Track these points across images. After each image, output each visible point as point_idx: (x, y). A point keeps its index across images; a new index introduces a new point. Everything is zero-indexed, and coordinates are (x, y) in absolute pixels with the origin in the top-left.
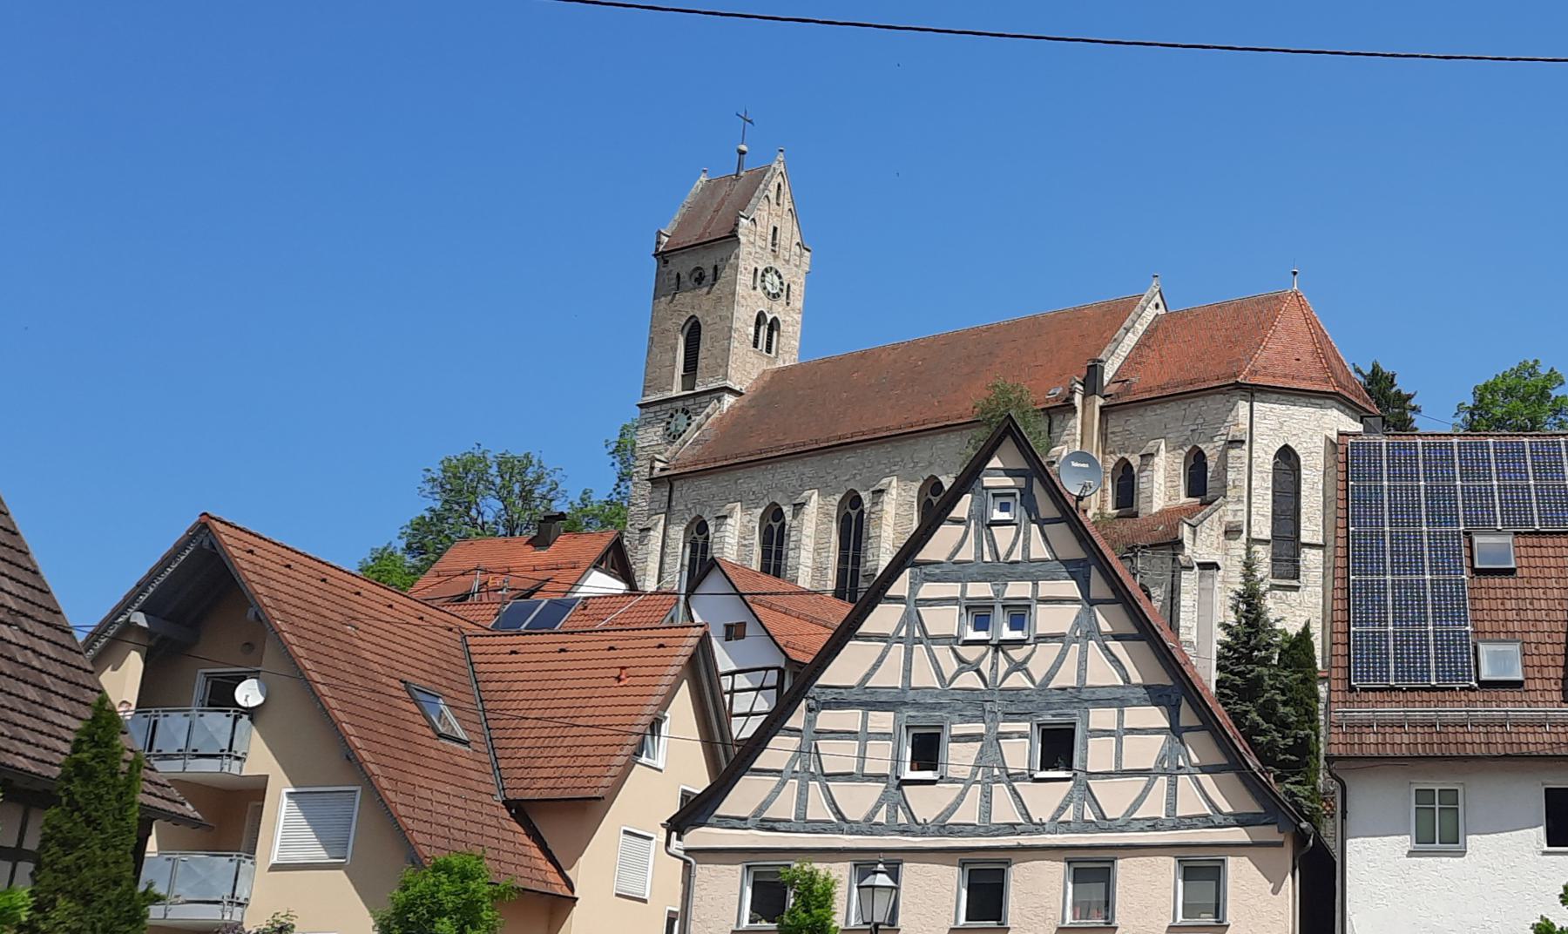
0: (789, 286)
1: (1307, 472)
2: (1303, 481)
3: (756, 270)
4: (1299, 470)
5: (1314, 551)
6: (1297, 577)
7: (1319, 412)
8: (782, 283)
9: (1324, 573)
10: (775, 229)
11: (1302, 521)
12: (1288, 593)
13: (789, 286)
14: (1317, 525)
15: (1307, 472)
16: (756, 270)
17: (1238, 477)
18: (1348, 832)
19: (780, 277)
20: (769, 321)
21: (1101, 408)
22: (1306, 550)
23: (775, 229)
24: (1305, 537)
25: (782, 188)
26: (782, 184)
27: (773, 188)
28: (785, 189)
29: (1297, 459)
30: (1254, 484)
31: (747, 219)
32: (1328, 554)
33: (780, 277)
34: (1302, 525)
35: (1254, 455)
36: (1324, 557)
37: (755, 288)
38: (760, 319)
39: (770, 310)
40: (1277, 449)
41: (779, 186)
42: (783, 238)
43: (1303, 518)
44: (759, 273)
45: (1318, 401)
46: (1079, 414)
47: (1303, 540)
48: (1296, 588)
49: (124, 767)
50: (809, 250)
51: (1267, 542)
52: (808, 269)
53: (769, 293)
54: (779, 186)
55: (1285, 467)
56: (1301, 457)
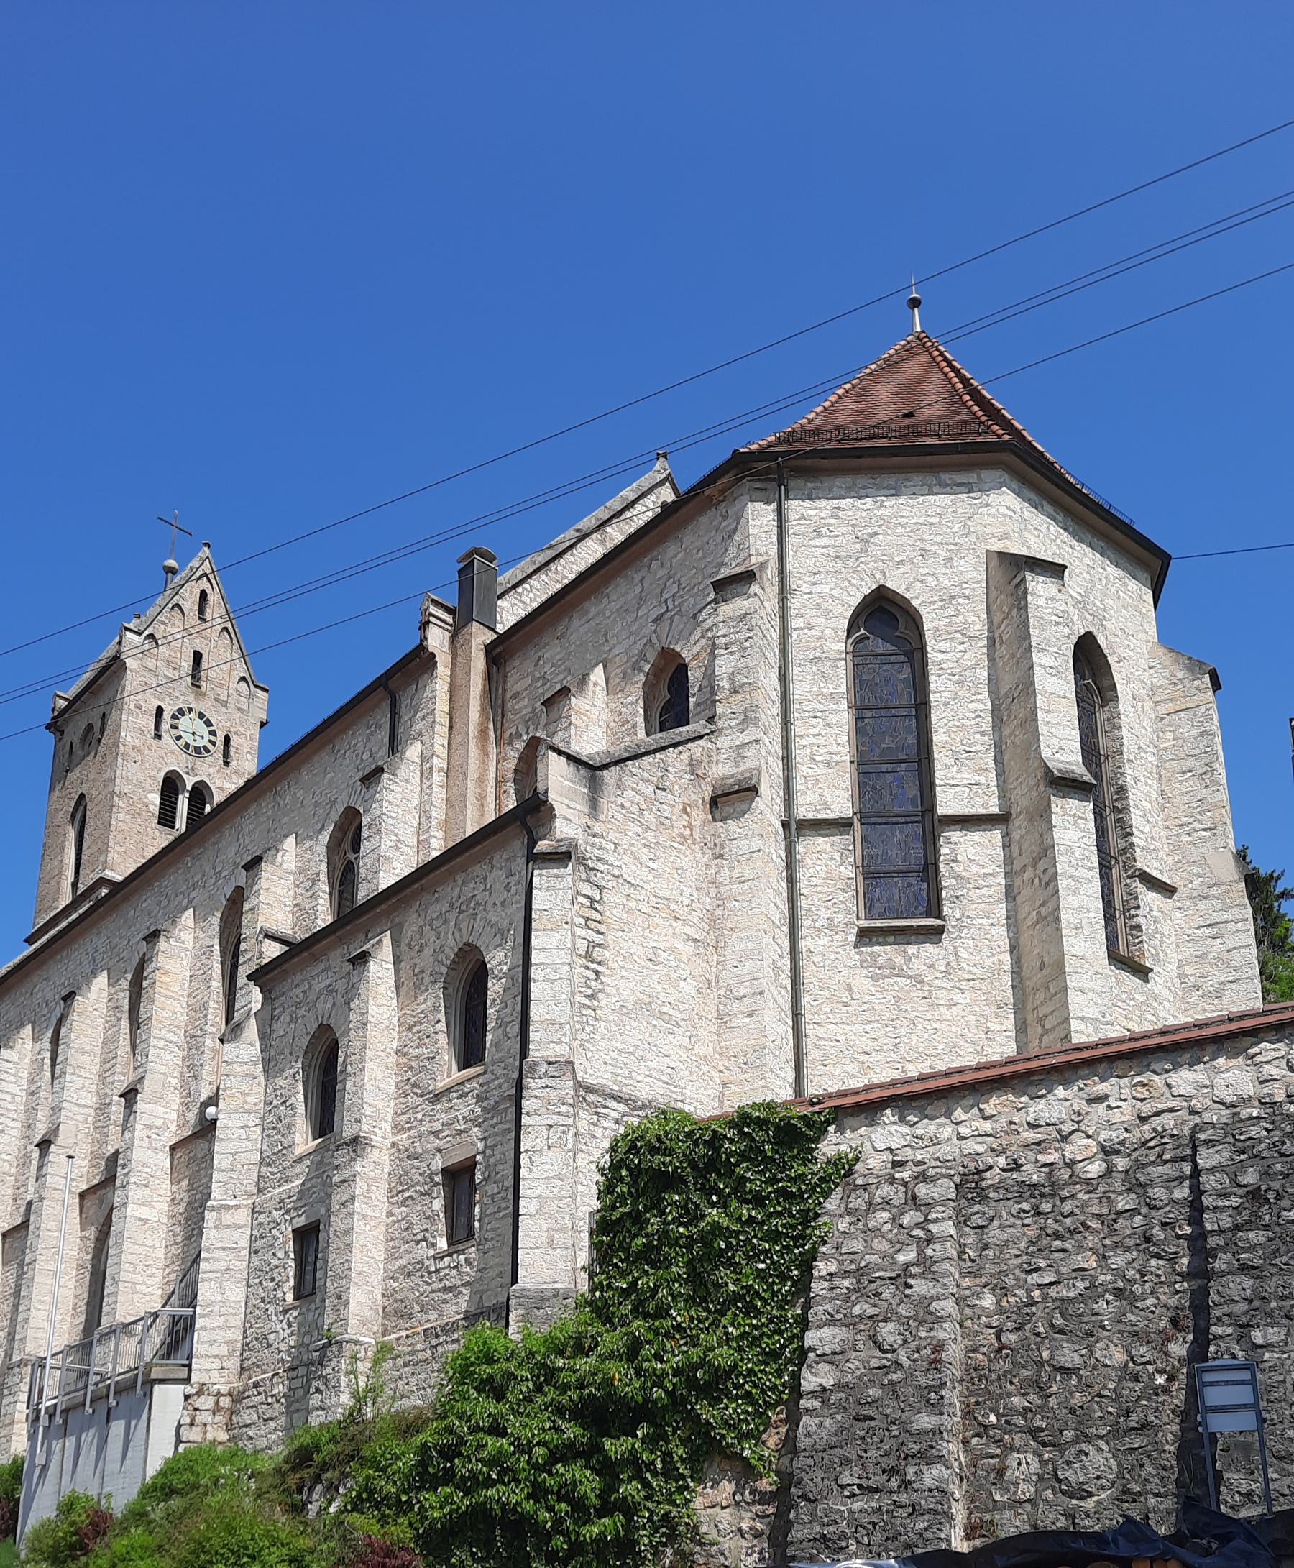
0: (227, 739)
1: (941, 646)
2: (932, 669)
3: (160, 711)
4: (922, 648)
5: (977, 836)
6: (934, 908)
7: (964, 501)
8: (213, 733)
9: (1009, 888)
10: (198, 657)
11: (938, 765)
12: (912, 949)
13: (227, 739)
14: (979, 771)
15: (941, 646)
16: (160, 711)
17: (743, 662)
18: (111, 1417)
19: (208, 723)
20: (189, 787)
21: (489, 649)
22: (955, 835)
23: (198, 657)
24: (948, 803)
25: (210, 597)
26: (209, 591)
27: (189, 599)
28: (214, 598)
29: (914, 620)
30: (796, 690)
31: (140, 634)
32: (1016, 835)
33: (208, 723)
34: (939, 774)
35: (794, 622)
36: (1005, 846)
37: (158, 737)
38: (171, 785)
39: (191, 770)
40: (855, 601)
41: (203, 595)
42: (214, 670)
43: (941, 759)
44: (167, 715)
45: (959, 478)
46: (442, 670)
47: (941, 811)
48: (934, 934)
49: (74, 1538)
50: (266, 691)
51: (839, 826)
52: (264, 718)
53: (187, 746)
54: (203, 595)
55: (880, 646)
56: (924, 612)
